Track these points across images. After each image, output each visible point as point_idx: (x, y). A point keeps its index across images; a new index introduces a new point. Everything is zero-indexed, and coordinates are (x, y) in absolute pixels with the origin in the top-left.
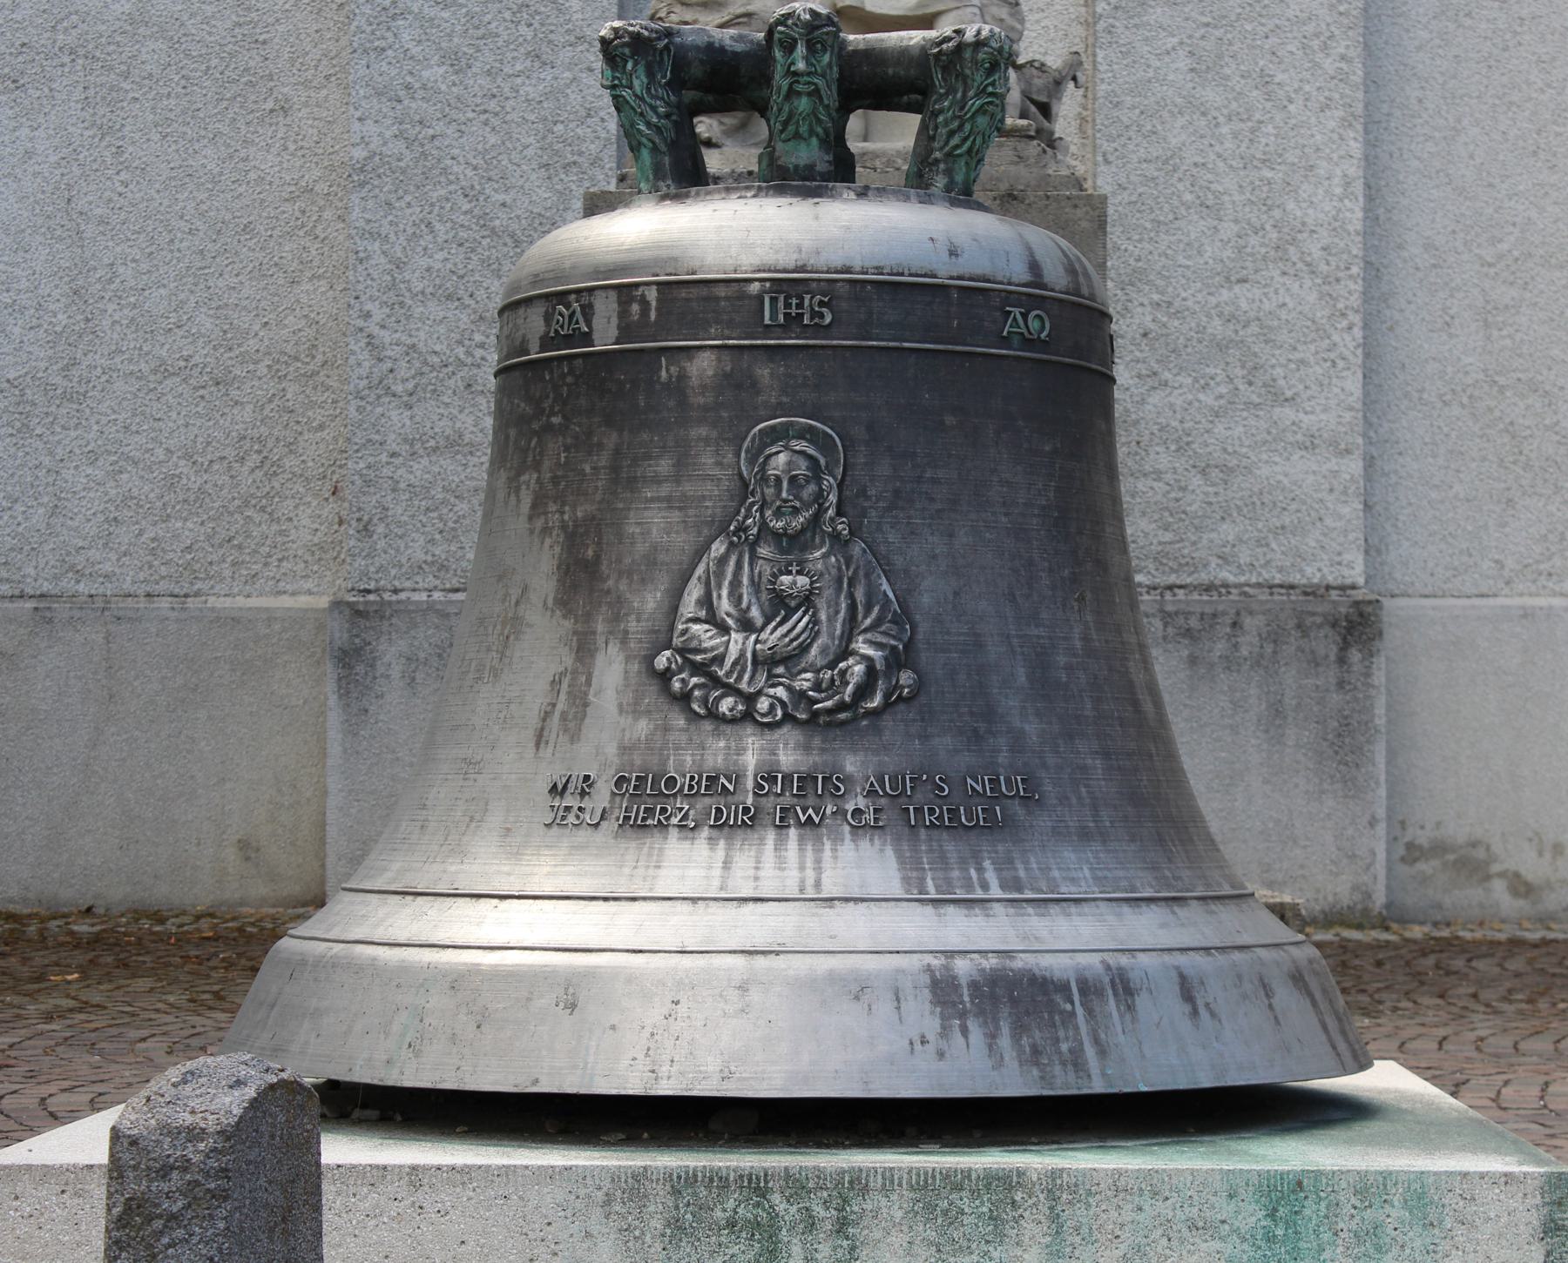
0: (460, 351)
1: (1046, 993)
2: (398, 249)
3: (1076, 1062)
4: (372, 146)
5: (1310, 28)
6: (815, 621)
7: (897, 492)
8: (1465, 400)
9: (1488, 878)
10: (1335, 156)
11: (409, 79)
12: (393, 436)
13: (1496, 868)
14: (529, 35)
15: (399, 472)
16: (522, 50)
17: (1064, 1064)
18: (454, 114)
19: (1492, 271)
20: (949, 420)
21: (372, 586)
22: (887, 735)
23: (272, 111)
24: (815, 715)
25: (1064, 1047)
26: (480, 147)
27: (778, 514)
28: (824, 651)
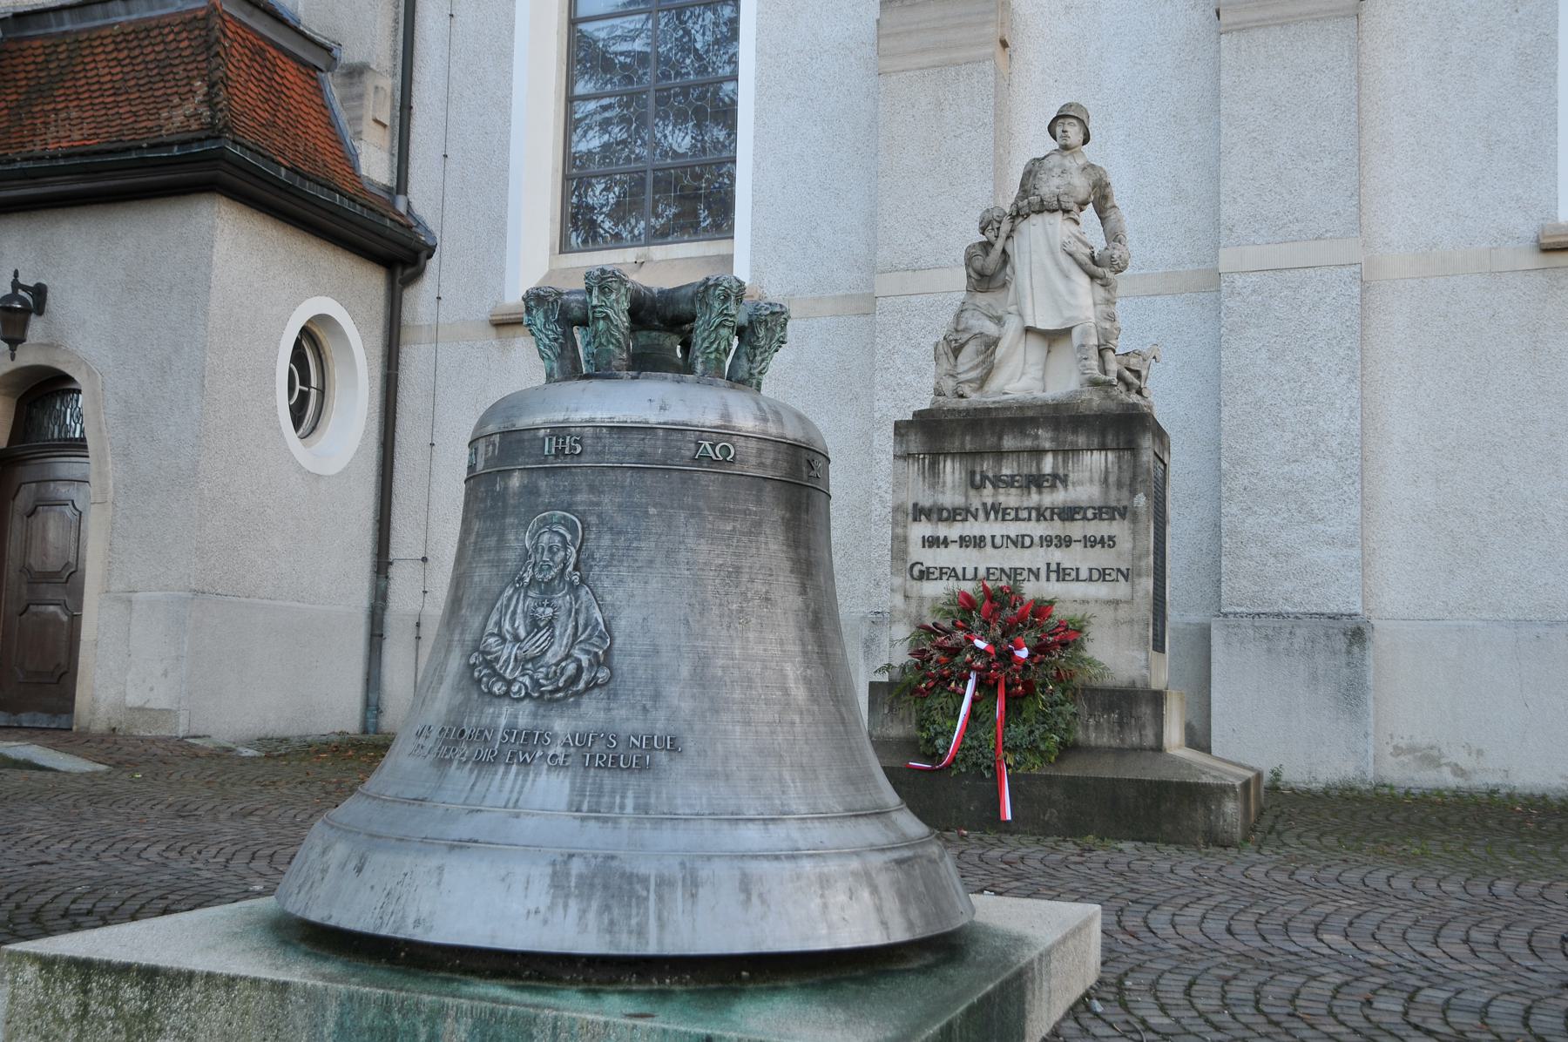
1: (631, 883)
3: (641, 932)
5: (1331, 335)
6: (553, 636)
7: (612, 555)
9: (1440, 766)
13: (1443, 761)
17: (630, 932)
20: (652, 511)
22: (583, 709)
24: (542, 693)
25: (634, 921)
27: (541, 570)
28: (554, 655)
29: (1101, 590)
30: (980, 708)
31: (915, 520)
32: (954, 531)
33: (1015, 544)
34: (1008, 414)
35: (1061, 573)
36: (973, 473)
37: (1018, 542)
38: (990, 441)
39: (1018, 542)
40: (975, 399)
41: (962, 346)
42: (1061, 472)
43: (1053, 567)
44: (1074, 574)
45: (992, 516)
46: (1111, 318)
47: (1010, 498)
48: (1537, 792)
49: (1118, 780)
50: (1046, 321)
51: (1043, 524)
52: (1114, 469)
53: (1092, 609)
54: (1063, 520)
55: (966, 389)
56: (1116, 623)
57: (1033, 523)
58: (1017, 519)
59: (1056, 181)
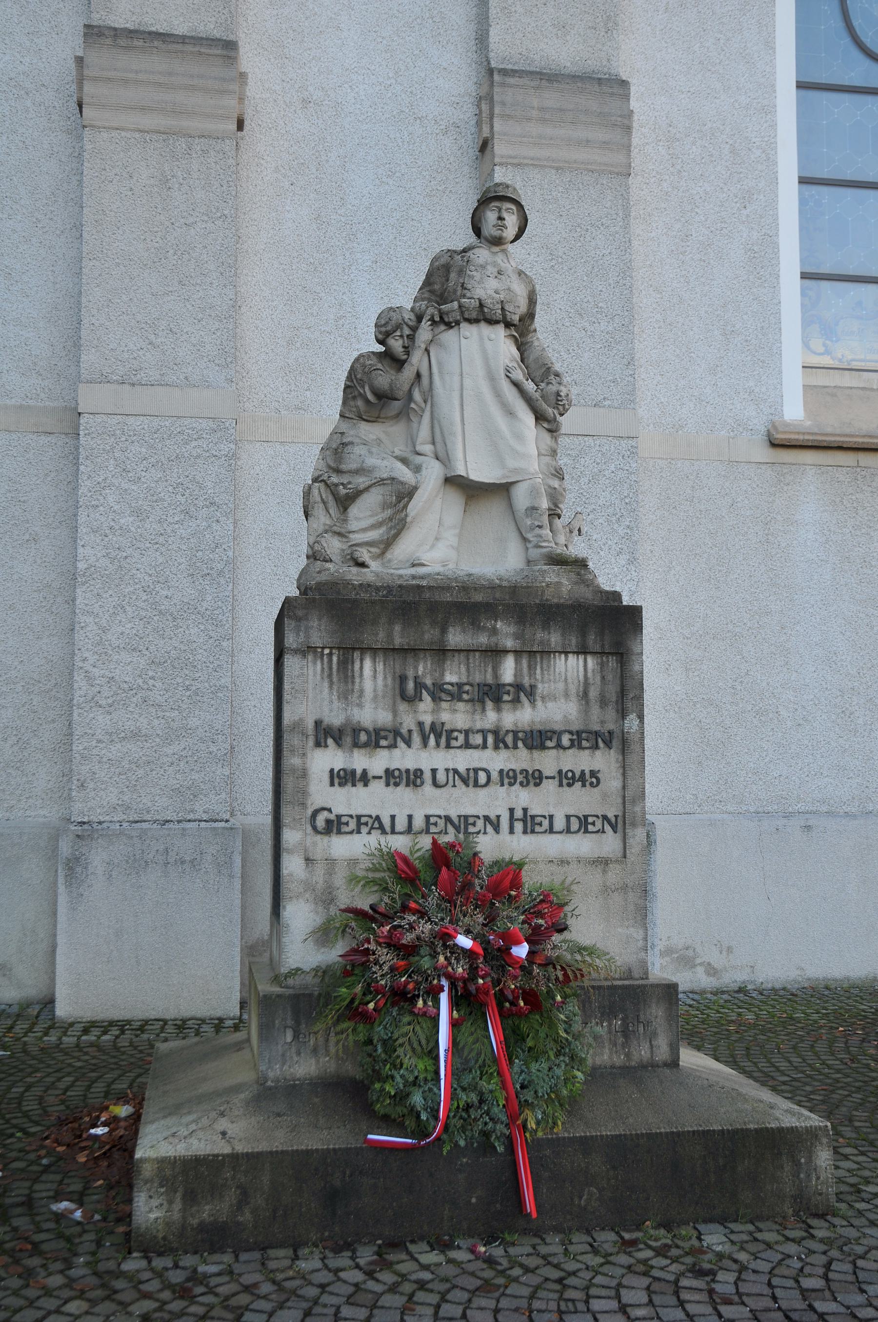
0: (140, 681)
2: (104, 621)
4: (90, 562)
8: (676, 709)
10: (625, 580)
11: (112, 524)
12: (100, 731)
13: (698, 961)
14: (183, 500)
15: (103, 752)
16: (179, 509)
18: (138, 545)
19: (689, 641)
21: (86, 820)
23: (28, 541)
26: (153, 564)
29: (581, 845)
30: (466, 1038)
31: (318, 744)
32: (378, 762)
33: (465, 782)
34: (448, 597)
35: (530, 823)
36: (403, 679)
37: (469, 779)
38: (430, 634)
39: (469, 779)
40: (376, 570)
41: (356, 494)
42: (526, 681)
43: (519, 814)
44: (546, 823)
45: (432, 741)
46: (559, 474)
47: (457, 716)
48: (778, 986)
49: (678, 1134)
50: (481, 472)
51: (504, 754)
52: (596, 680)
53: (574, 872)
54: (530, 747)
55: (364, 555)
56: (606, 890)
57: (489, 752)
58: (467, 745)
59: (492, 284)
